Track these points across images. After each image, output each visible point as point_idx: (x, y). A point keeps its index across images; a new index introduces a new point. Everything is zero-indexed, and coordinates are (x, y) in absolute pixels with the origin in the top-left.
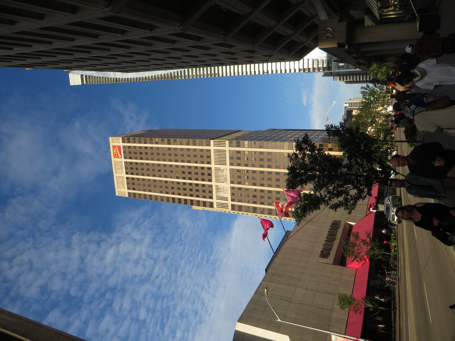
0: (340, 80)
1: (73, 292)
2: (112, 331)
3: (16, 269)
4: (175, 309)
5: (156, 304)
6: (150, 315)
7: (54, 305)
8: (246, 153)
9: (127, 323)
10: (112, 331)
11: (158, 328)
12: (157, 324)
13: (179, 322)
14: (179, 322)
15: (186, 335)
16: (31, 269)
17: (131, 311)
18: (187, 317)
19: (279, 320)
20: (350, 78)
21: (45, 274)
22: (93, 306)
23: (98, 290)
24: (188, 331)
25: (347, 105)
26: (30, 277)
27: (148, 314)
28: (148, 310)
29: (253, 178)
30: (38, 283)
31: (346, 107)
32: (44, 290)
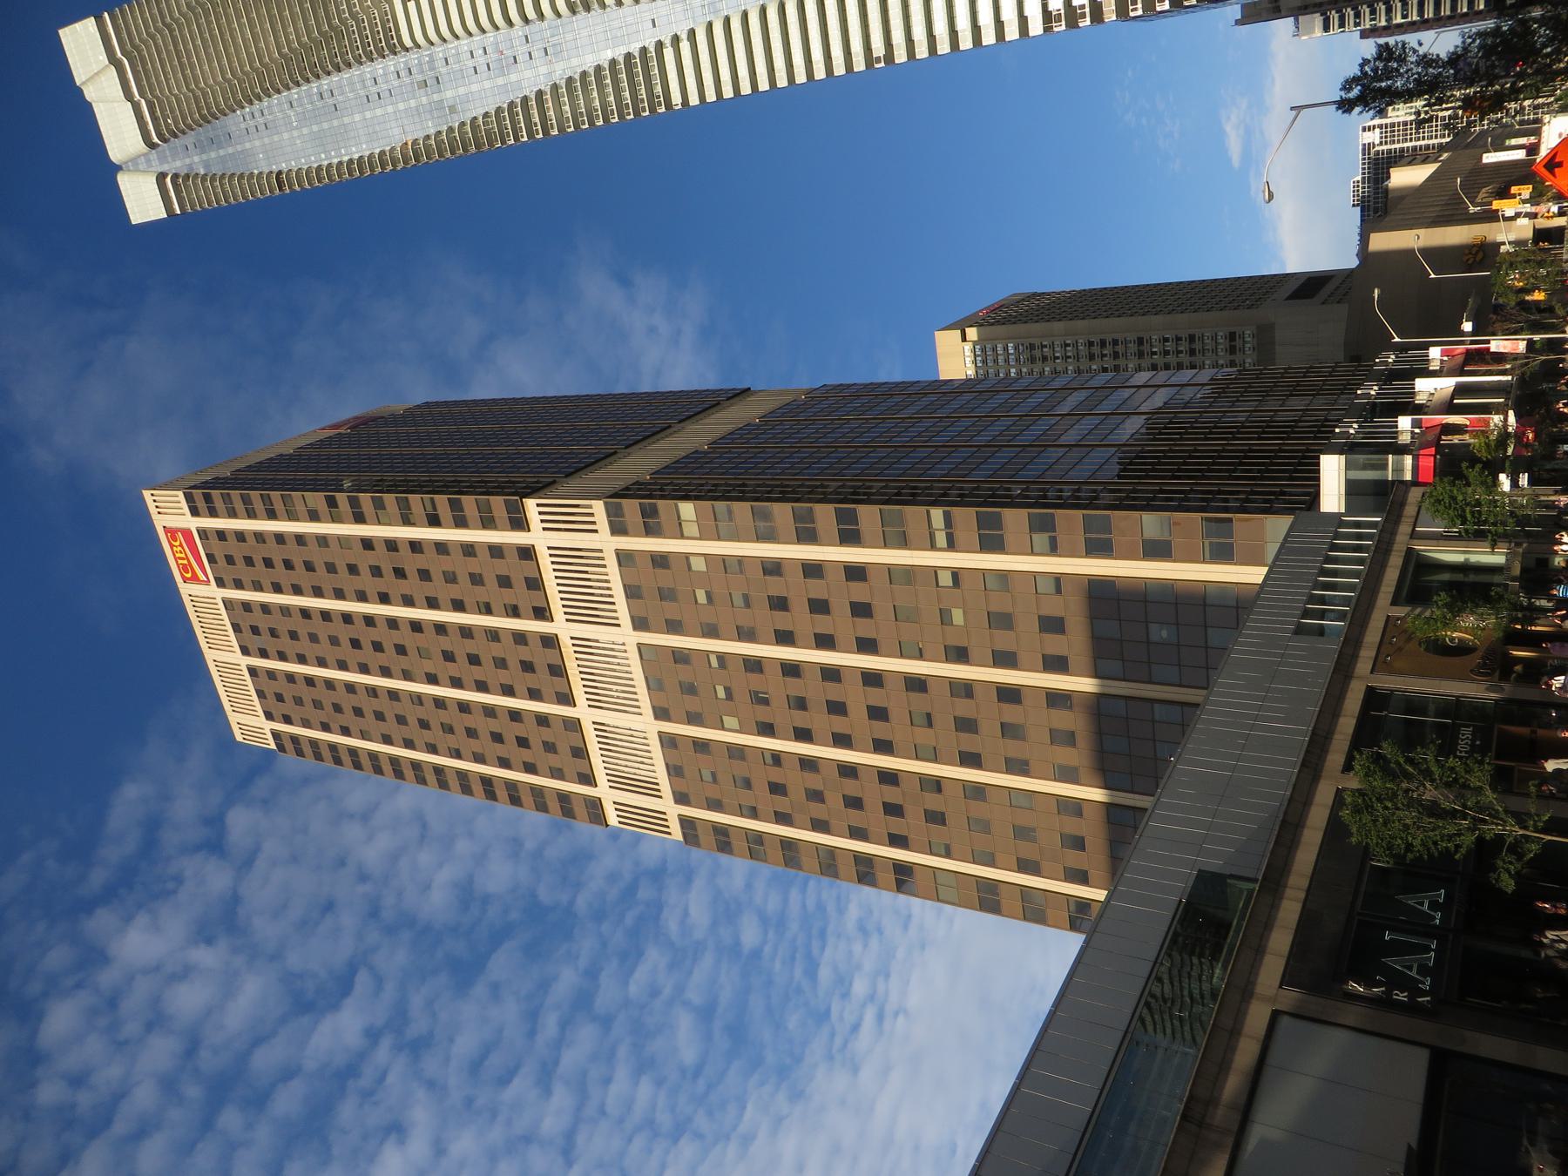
0: (1326, 28)
1: (544, 895)
2: (667, 991)
3: (384, 842)
4: (841, 911)
5: (785, 901)
6: (771, 935)
7: (499, 936)
8: (699, 565)
9: (707, 961)
10: (667, 991)
11: (798, 972)
12: (793, 958)
13: (857, 948)
14: (857, 948)
15: (881, 987)
16: (423, 838)
17: (714, 924)
18: (880, 931)
19: (1397, 339)
20: (1373, 12)
21: (463, 846)
22: (605, 927)
23: (613, 877)
24: (887, 976)
25: (1374, 137)
26: (425, 858)
27: (766, 932)
28: (764, 920)
29: (757, 696)
30: (445, 875)
31: (1367, 148)
32: (466, 894)
